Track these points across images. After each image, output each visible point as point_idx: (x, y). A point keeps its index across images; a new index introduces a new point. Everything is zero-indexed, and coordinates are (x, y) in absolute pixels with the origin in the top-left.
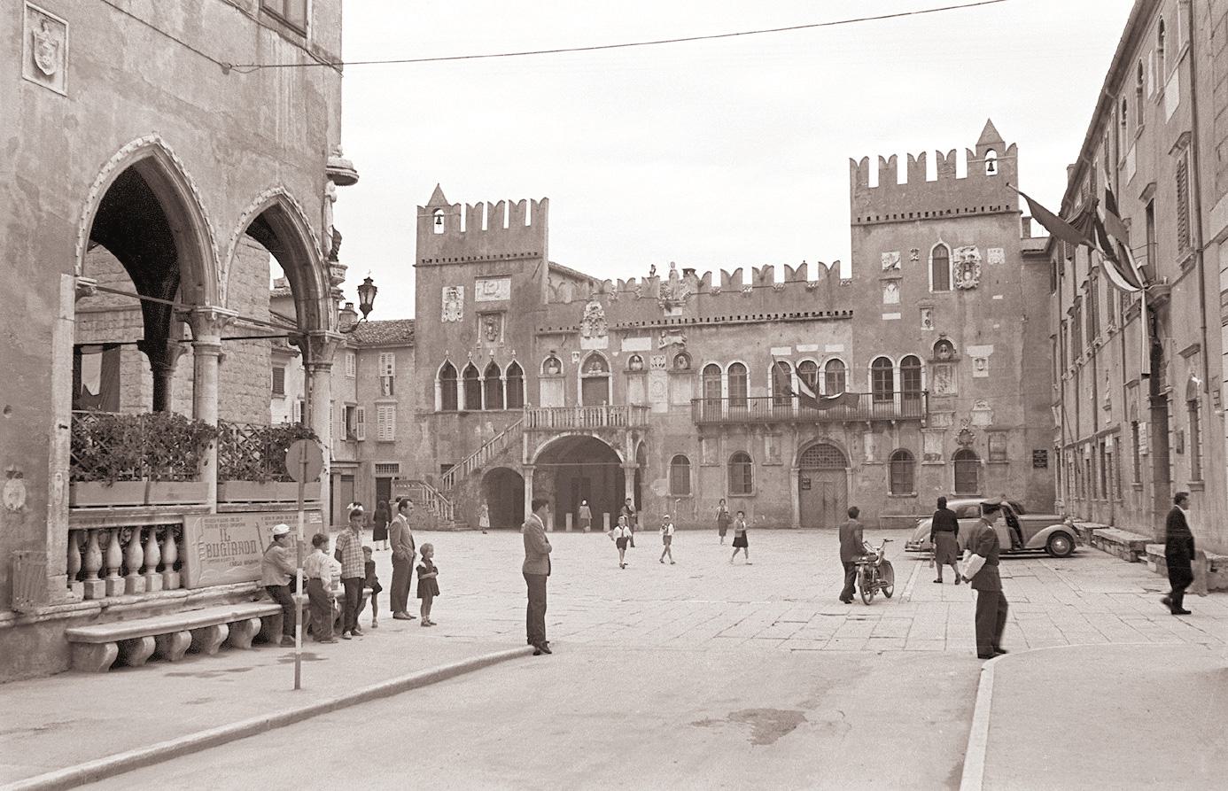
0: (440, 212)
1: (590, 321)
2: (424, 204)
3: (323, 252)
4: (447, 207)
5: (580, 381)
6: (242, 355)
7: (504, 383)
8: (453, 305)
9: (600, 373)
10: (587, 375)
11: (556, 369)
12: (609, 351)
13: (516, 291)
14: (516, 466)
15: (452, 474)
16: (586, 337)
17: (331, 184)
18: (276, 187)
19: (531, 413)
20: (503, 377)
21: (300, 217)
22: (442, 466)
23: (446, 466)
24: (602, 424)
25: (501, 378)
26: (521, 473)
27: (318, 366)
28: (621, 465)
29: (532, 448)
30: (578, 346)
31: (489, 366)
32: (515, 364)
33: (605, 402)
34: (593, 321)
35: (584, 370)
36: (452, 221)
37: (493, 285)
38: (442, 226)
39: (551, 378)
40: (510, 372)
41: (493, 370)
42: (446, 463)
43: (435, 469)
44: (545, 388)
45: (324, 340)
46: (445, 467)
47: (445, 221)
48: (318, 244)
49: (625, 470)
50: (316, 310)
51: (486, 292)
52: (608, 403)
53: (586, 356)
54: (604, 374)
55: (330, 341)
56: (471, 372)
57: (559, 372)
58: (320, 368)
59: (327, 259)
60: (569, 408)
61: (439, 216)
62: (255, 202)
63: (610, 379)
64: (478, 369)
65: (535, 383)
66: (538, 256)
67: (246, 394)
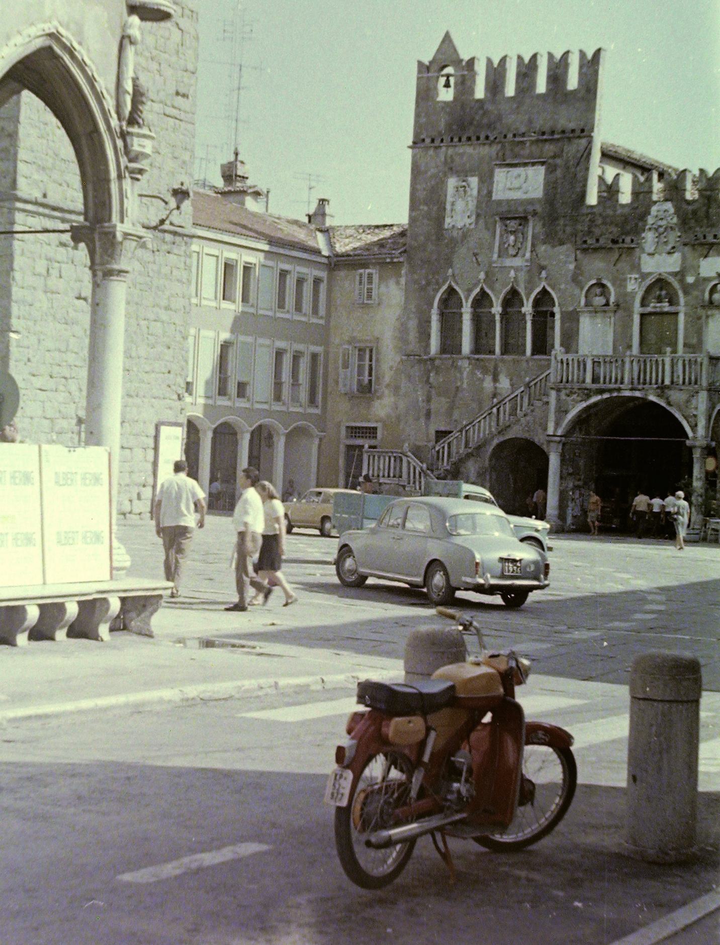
0: (450, 70)
1: (656, 230)
2: (426, 59)
3: (118, 113)
4: (457, 62)
5: (636, 319)
6: (151, 266)
7: (498, 318)
8: (460, 205)
9: (666, 307)
10: (649, 309)
11: (603, 301)
12: (680, 275)
13: (550, 186)
14: (539, 439)
15: (449, 444)
16: (649, 254)
17: (135, 20)
18: (45, 22)
19: (562, 362)
20: (497, 309)
21: (82, 66)
22: (437, 432)
23: (442, 432)
24: (663, 381)
25: (523, 310)
26: (545, 447)
27: (108, 274)
28: (688, 443)
29: (562, 411)
30: (636, 267)
31: (508, 293)
32: (482, 289)
33: (669, 349)
34: (661, 230)
35: (643, 304)
36: (465, 84)
37: (519, 176)
38: (451, 90)
39: (596, 312)
40: (537, 303)
41: (512, 299)
42: (443, 428)
43: (427, 436)
44: (586, 324)
45: (114, 236)
46: (441, 435)
47: (456, 83)
48: (110, 103)
49: (694, 451)
50: (107, 196)
51: (509, 185)
52: (674, 351)
53: (648, 282)
54: (672, 309)
55: (125, 239)
56: (482, 300)
57: (607, 304)
58: (112, 275)
59: (124, 124)
60: (617, 360)
61: (448, 76)
62: (12, 43)
63: (681, 318)
64: (494, 299)
65: (572, 318)
66: (585, 132)
67: (155, 321)
